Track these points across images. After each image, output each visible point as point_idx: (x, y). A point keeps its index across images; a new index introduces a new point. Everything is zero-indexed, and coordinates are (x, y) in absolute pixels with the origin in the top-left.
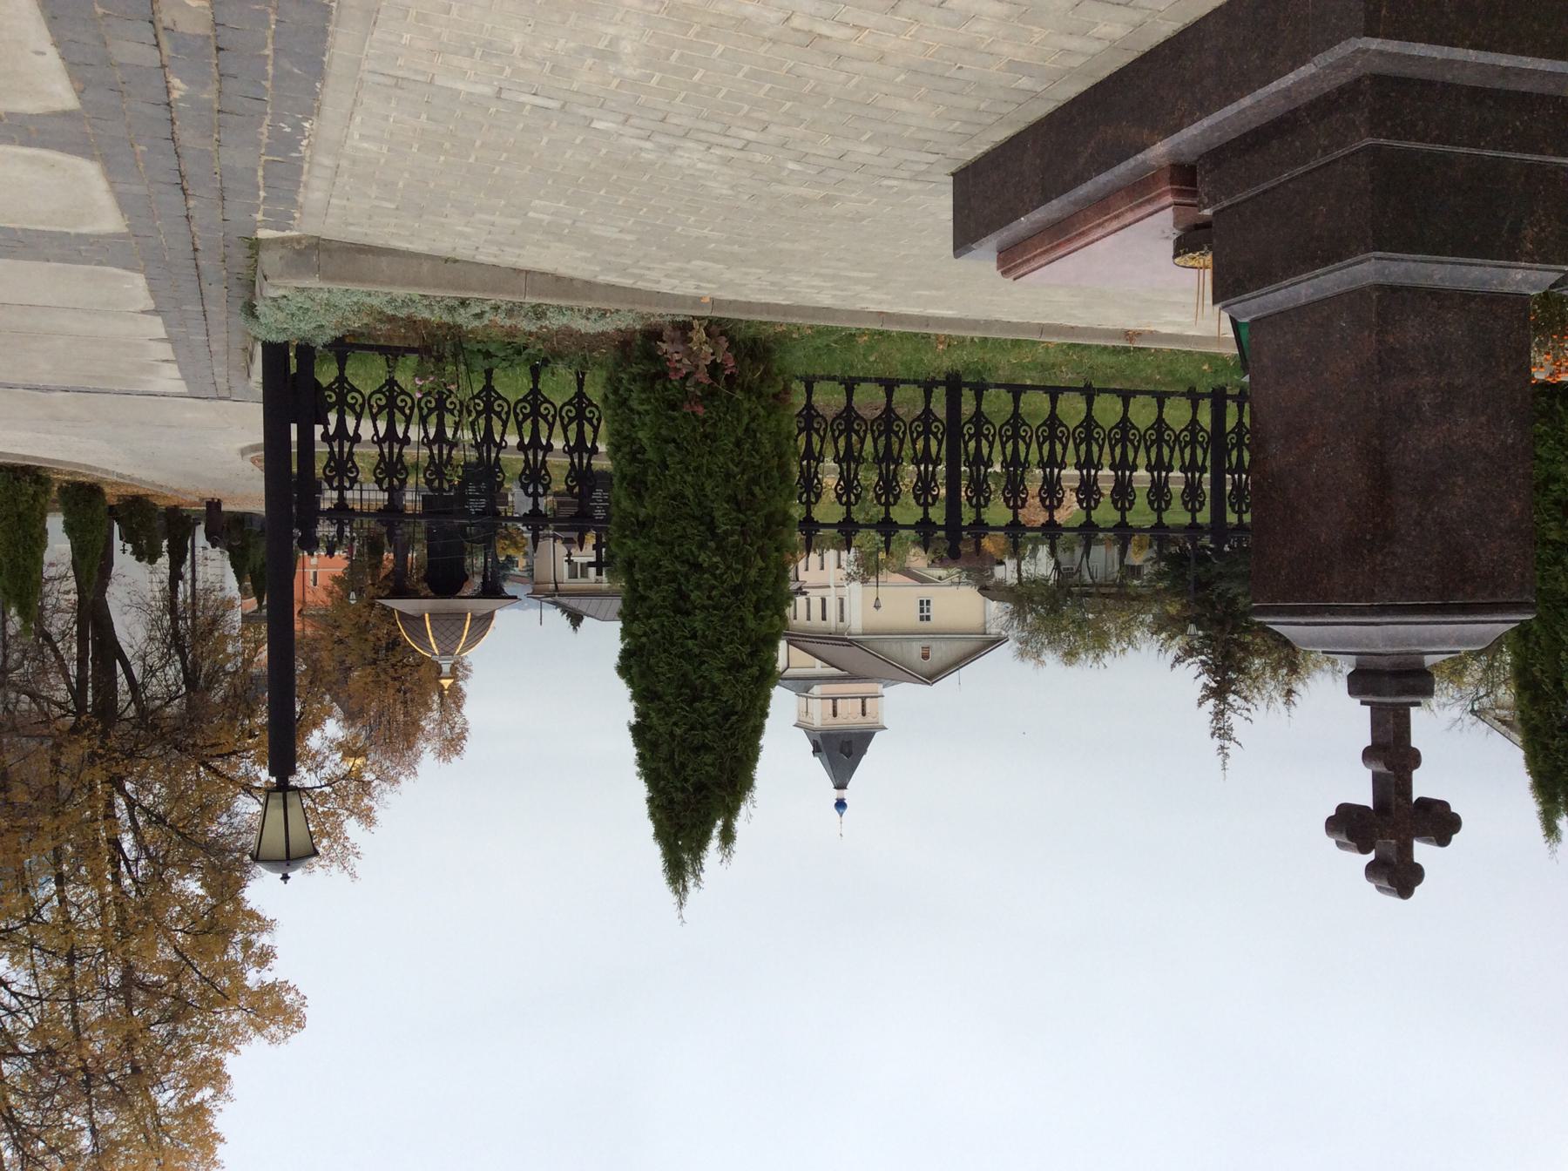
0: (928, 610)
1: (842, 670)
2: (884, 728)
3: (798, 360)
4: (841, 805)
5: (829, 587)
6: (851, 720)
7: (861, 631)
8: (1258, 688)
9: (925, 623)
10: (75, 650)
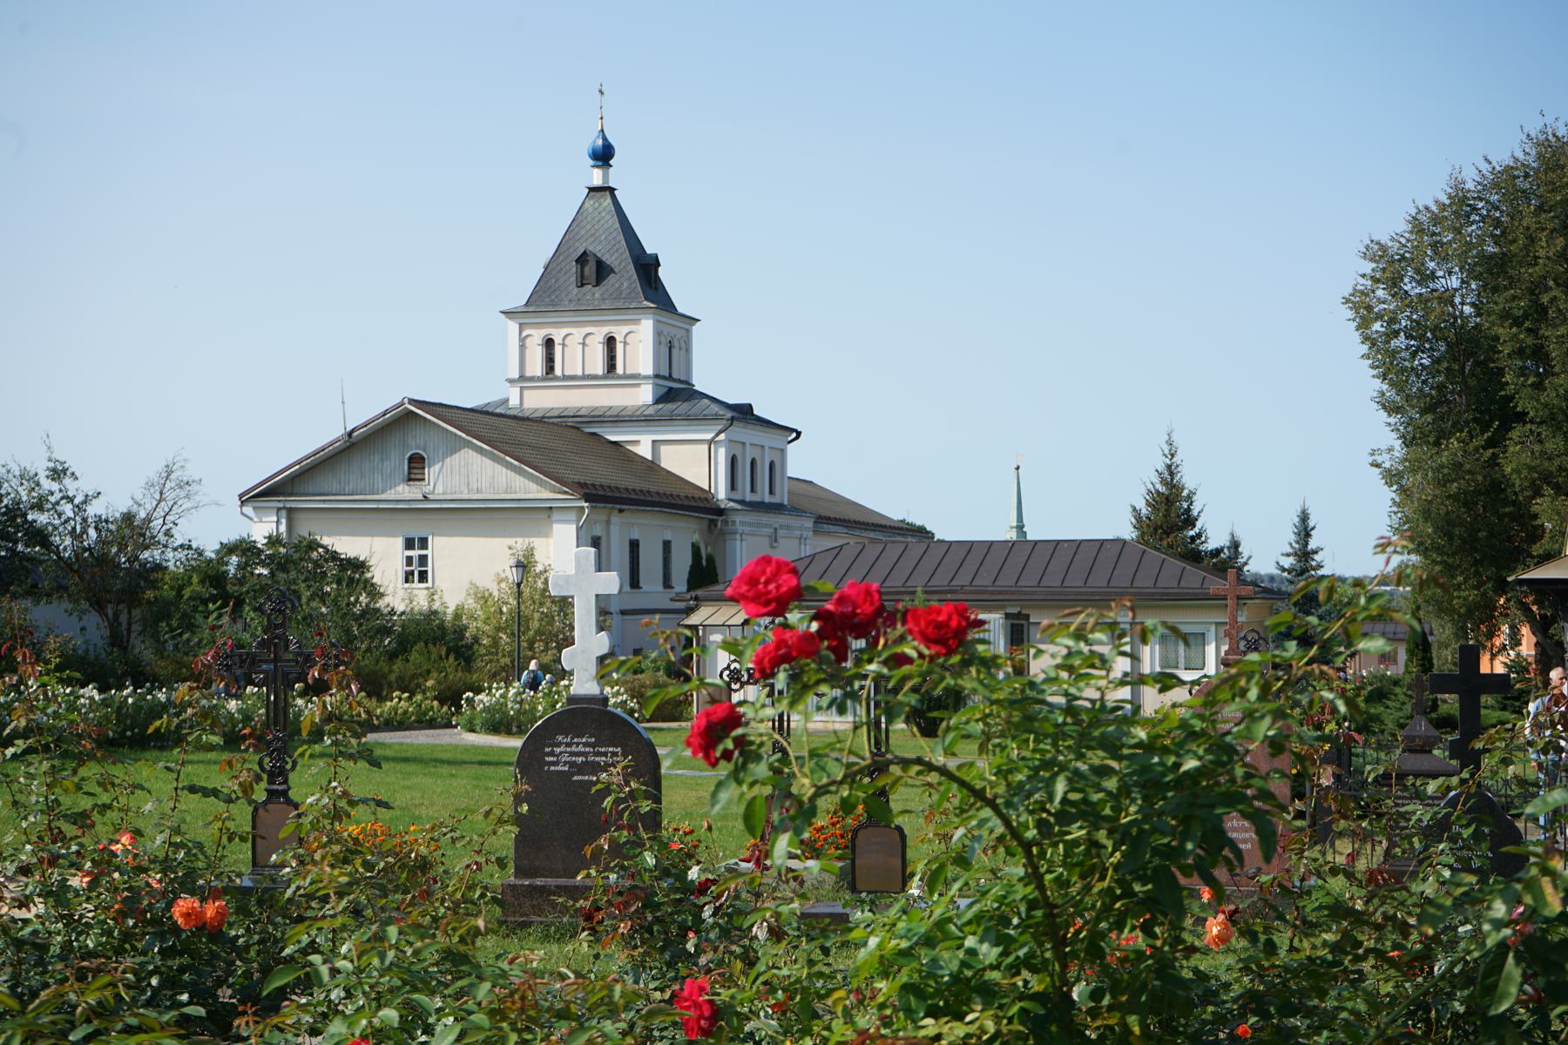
0: (409, 560)
1: (594, 434)
2: (508, 313)
3: (1367, 582)
4: (603, 156)
5: (623, 613)
6: (578, 333)
7: (555, 516)
8: (180, 589)
9: (416, 534)
10: (1049, 893)
